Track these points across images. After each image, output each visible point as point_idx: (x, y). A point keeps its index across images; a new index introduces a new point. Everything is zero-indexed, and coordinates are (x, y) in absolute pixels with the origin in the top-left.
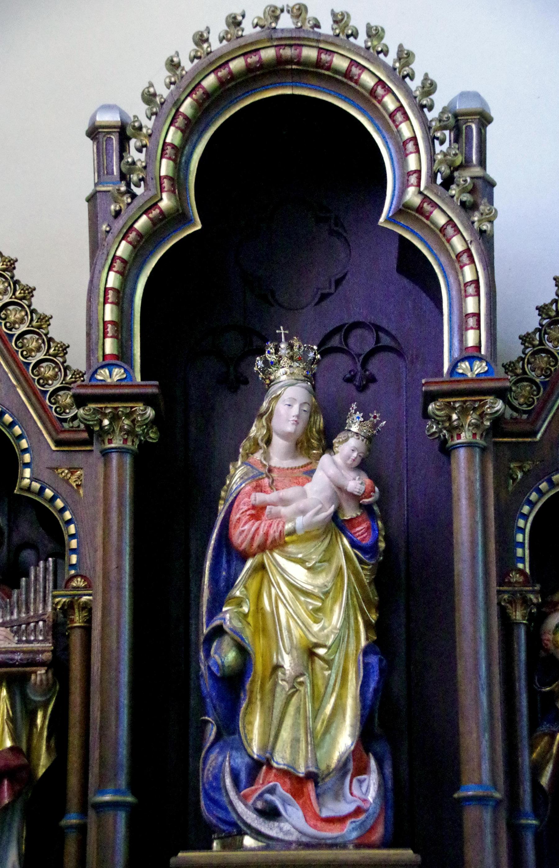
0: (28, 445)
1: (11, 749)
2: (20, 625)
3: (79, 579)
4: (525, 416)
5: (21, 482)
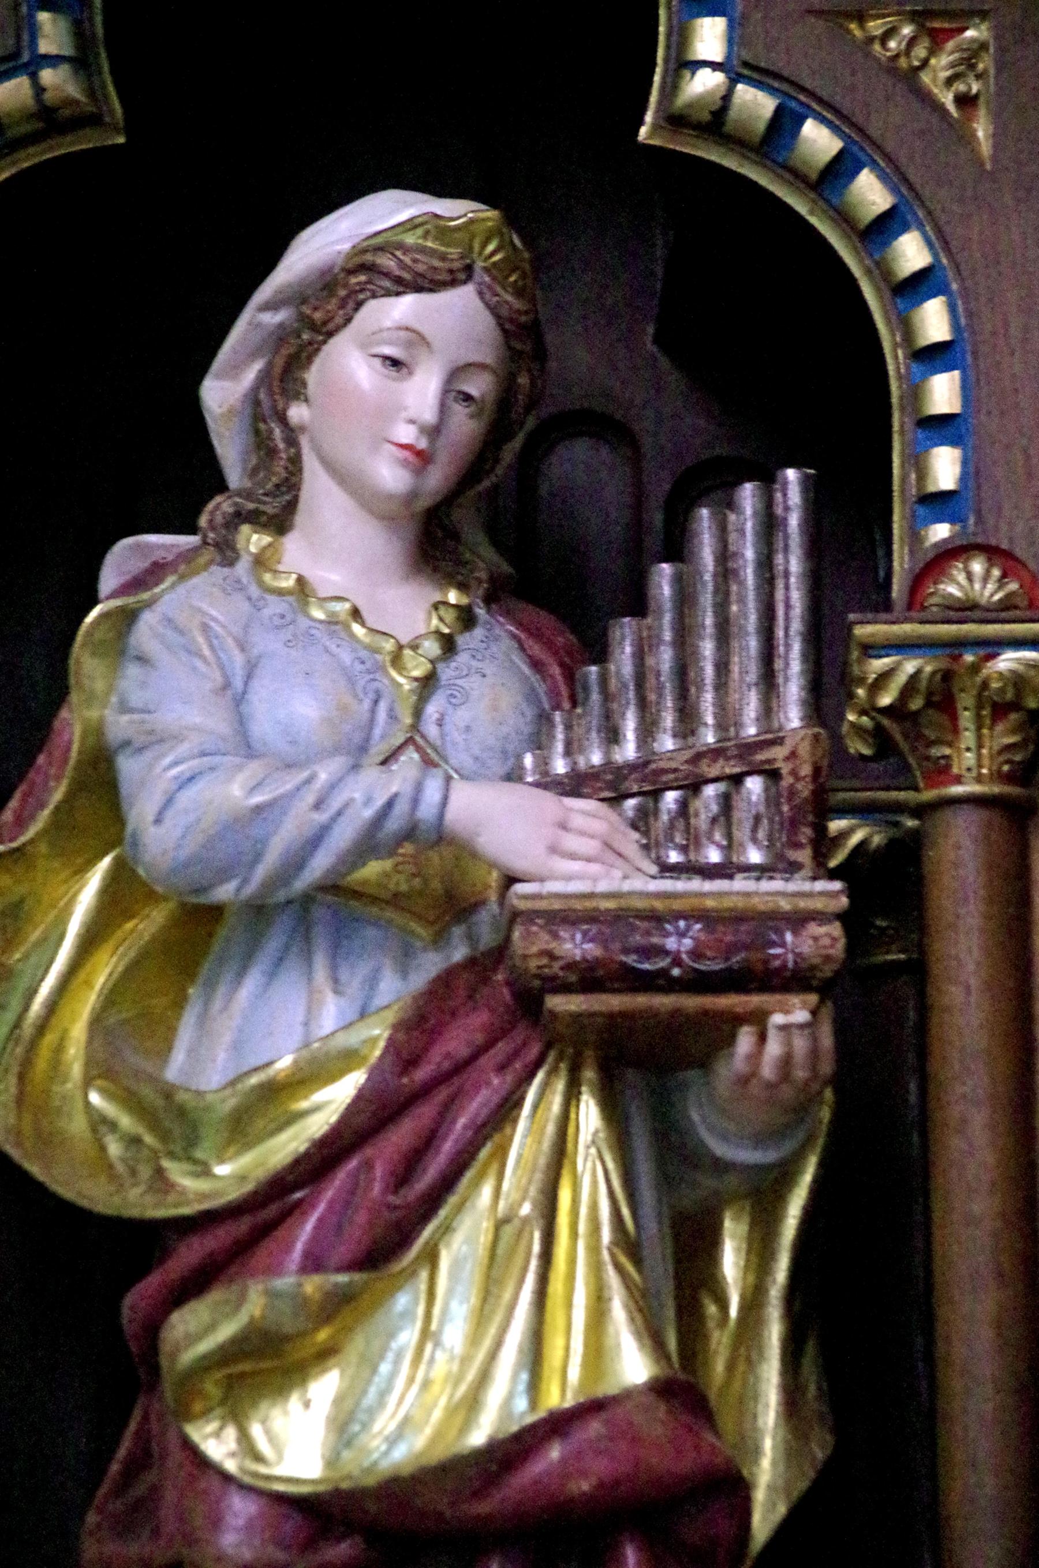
2: (656, 794)
3: (977, 567)
5: (671, 88)
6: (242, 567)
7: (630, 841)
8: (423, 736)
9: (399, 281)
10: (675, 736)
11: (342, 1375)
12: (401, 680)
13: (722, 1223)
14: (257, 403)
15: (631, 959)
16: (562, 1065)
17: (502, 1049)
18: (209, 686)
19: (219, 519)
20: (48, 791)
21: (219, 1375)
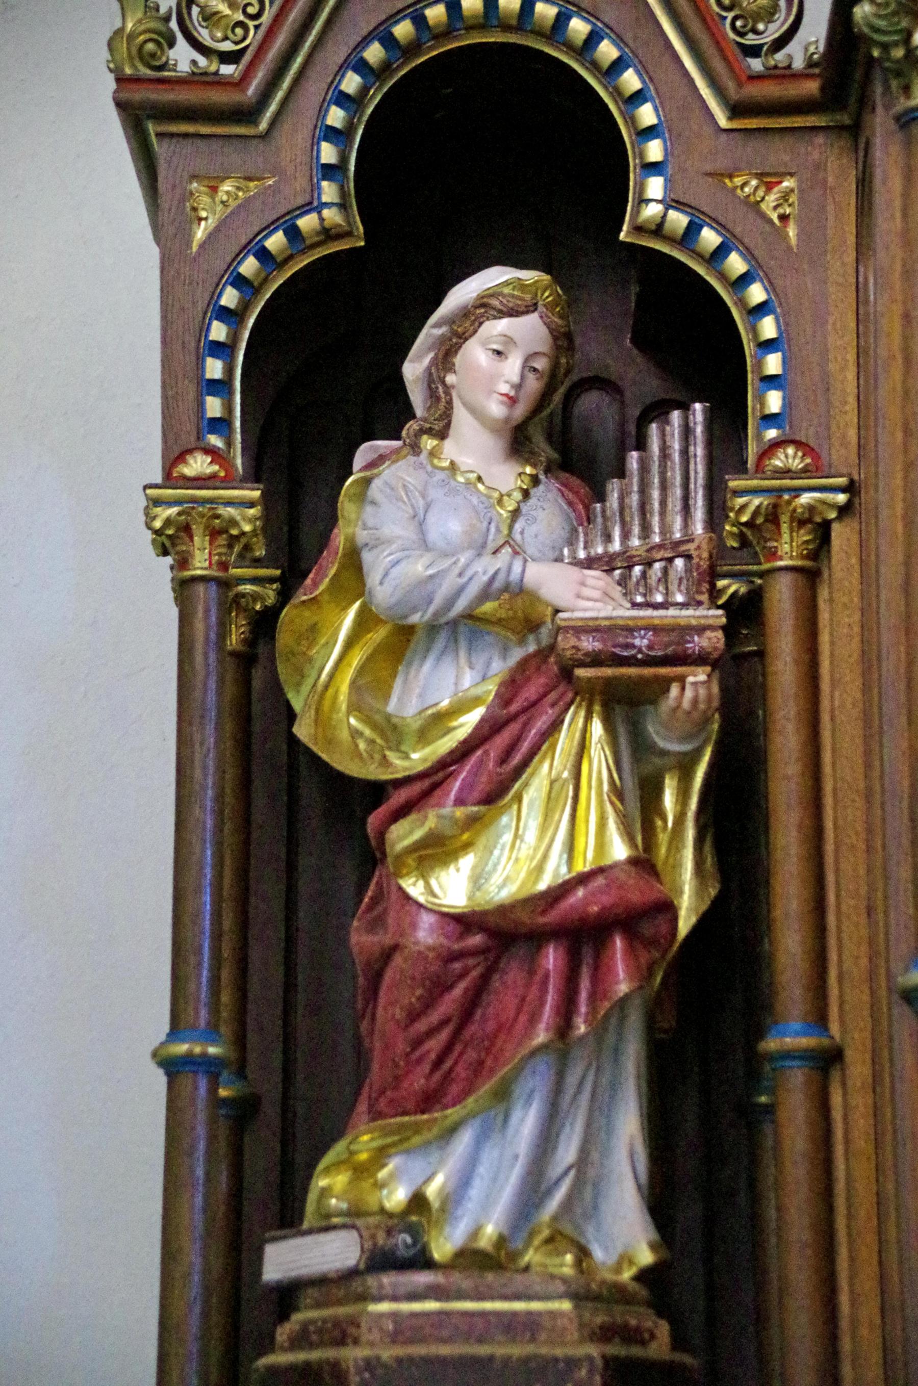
0: (658, 116)
1: (633, 861)
2: (630, 568)
4: (227, 70)
5: (637, 212)
6: (424, 456)
7: (617, 591)
8: (513, 540)
9: (500, 311)
10: (639, 538)
11: (475, 854)
12: (502, 512)
13: (664, 781)
14: (430, 374)
15: (617, 650)
16: (584, 703)
17: (553, 696)
18: (407, 515)
19: (412, 432)
20: (327, 568)
21: (416, 855)
